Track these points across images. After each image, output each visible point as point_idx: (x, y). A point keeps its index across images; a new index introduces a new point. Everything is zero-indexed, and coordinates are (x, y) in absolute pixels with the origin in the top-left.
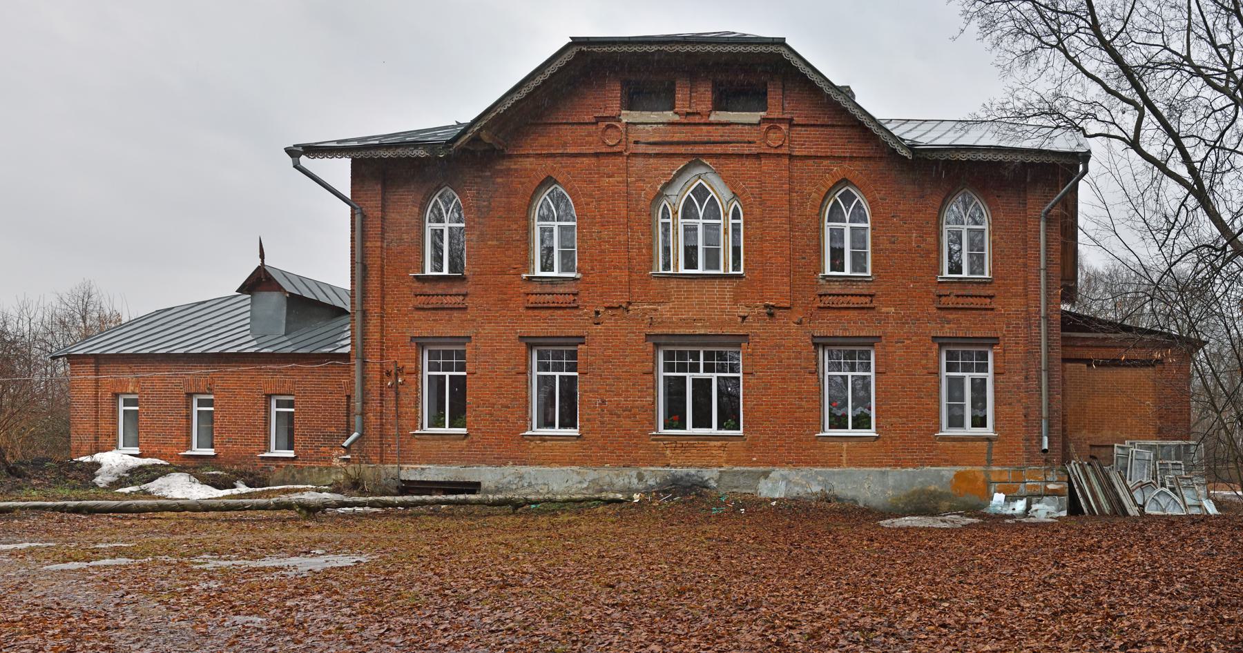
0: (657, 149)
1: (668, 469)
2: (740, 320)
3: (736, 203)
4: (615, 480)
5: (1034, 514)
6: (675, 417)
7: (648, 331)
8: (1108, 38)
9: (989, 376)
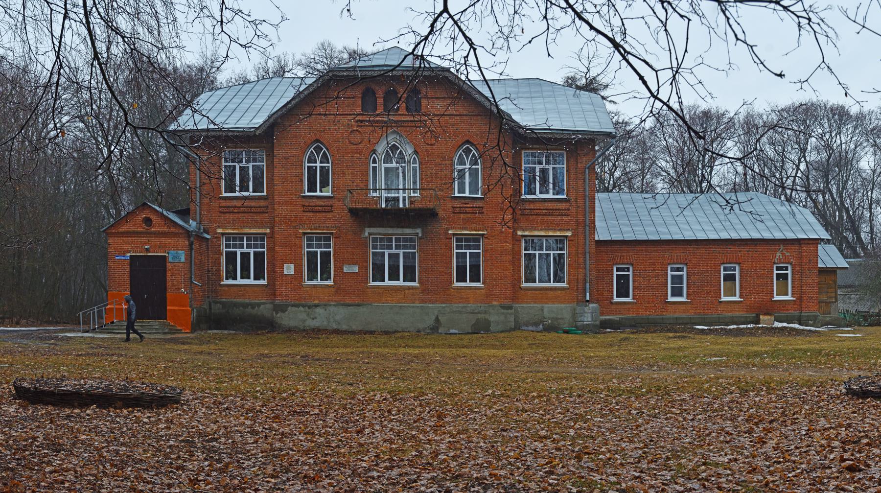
3: (414, 155)
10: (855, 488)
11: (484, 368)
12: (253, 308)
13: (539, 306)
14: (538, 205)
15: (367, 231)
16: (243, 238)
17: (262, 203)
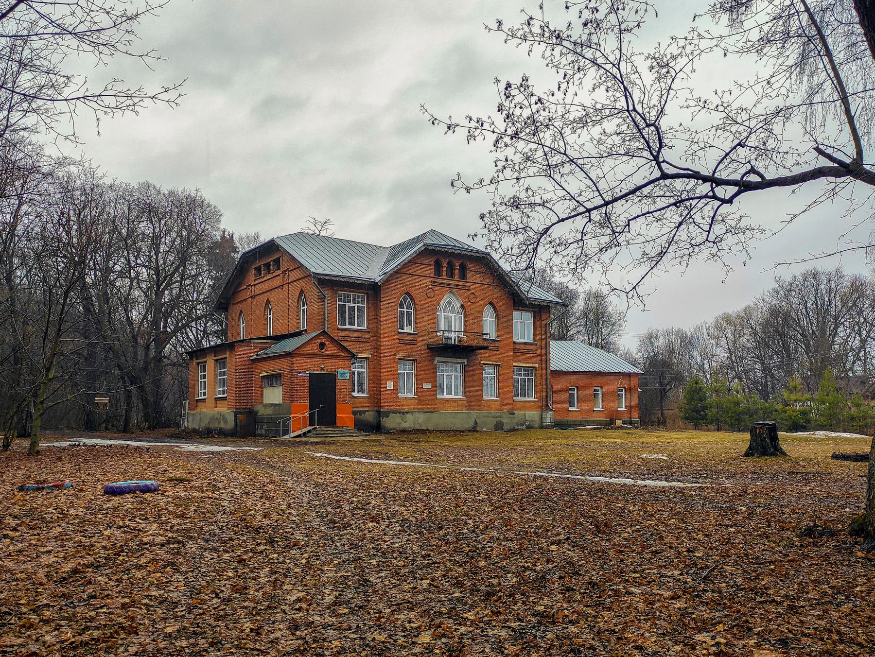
10: (520, 589)
11: (522, 167)
12: (361, 415)
13: (523, 412)
14: (347, 334)
15: (437, 359)
17: (366, 335)
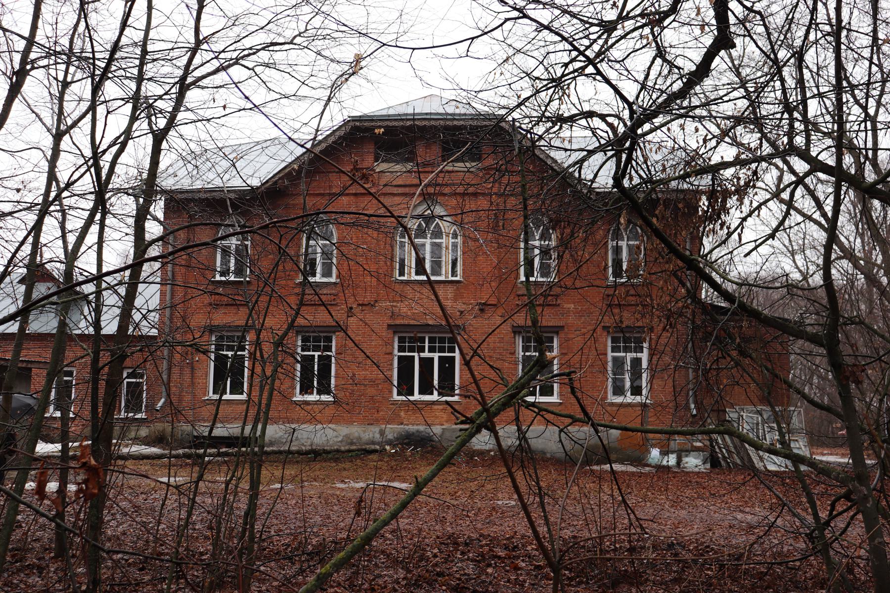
0: (401, 190)
1: (402, 426)
2: (458, 313)
4: (362, 435)
5: (686, 465)
6: (406, 387)
7: (391, 322)
8: (858, 98)
9: (644, 356)
16: (424, 338)
